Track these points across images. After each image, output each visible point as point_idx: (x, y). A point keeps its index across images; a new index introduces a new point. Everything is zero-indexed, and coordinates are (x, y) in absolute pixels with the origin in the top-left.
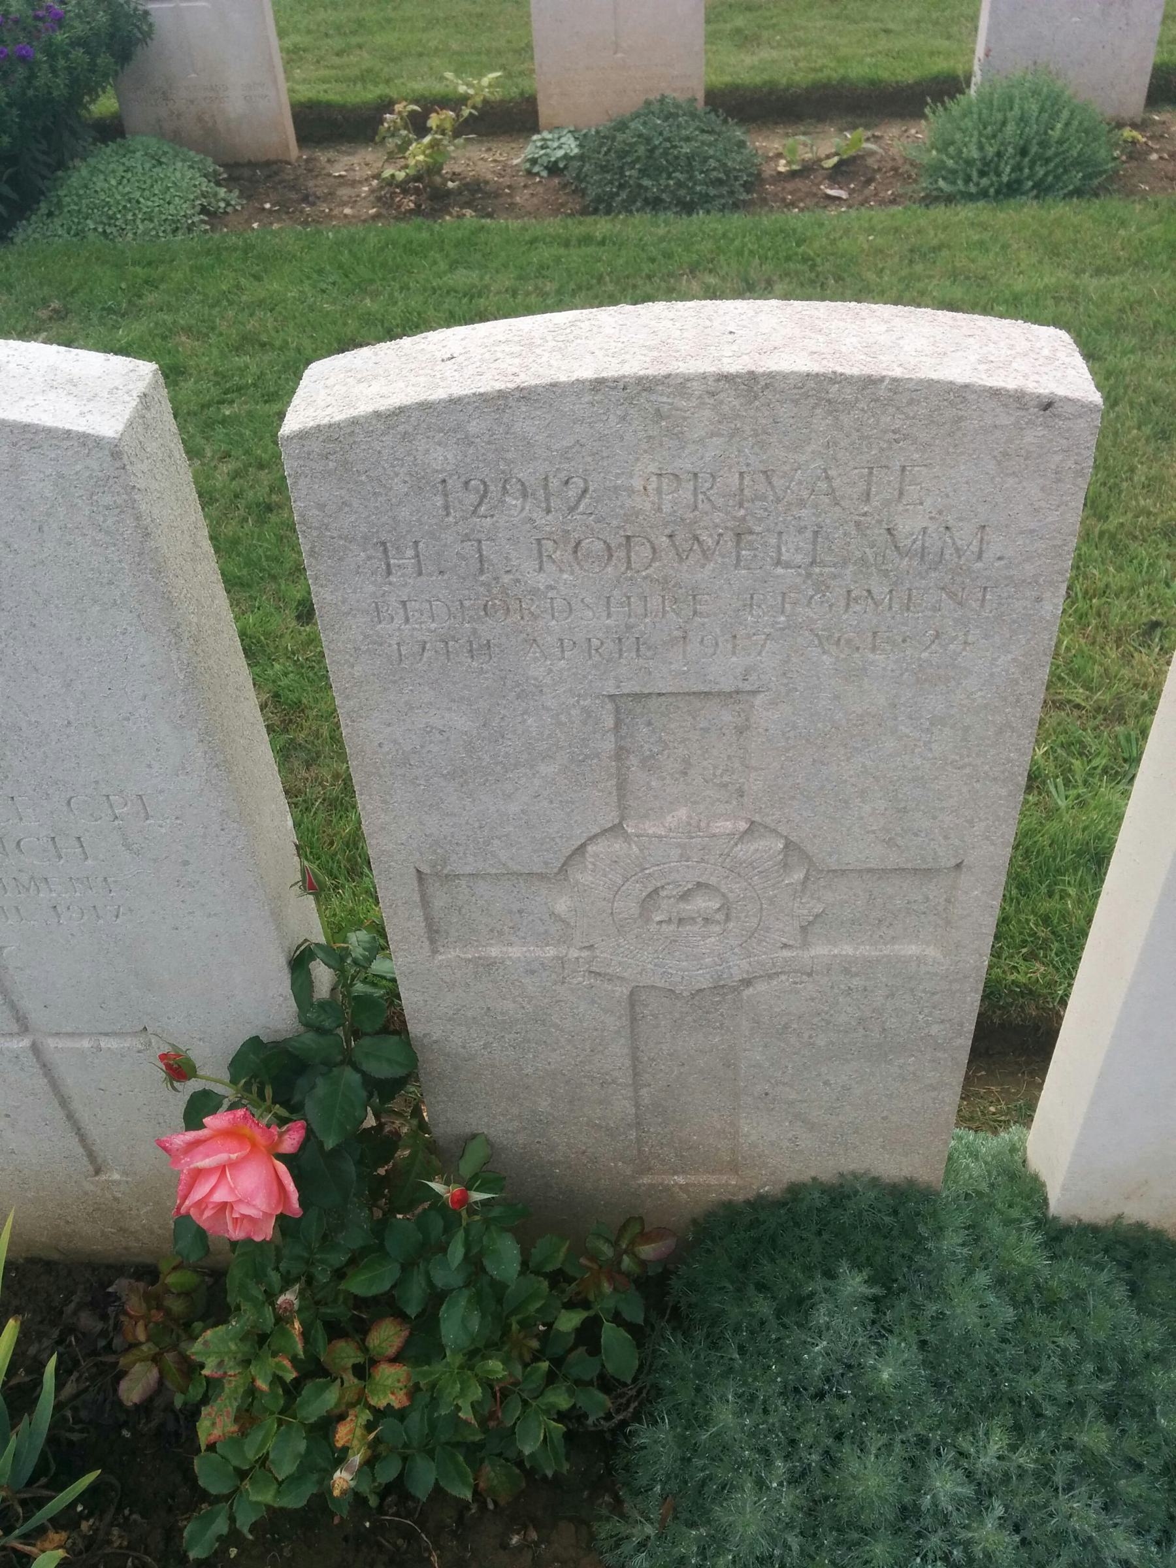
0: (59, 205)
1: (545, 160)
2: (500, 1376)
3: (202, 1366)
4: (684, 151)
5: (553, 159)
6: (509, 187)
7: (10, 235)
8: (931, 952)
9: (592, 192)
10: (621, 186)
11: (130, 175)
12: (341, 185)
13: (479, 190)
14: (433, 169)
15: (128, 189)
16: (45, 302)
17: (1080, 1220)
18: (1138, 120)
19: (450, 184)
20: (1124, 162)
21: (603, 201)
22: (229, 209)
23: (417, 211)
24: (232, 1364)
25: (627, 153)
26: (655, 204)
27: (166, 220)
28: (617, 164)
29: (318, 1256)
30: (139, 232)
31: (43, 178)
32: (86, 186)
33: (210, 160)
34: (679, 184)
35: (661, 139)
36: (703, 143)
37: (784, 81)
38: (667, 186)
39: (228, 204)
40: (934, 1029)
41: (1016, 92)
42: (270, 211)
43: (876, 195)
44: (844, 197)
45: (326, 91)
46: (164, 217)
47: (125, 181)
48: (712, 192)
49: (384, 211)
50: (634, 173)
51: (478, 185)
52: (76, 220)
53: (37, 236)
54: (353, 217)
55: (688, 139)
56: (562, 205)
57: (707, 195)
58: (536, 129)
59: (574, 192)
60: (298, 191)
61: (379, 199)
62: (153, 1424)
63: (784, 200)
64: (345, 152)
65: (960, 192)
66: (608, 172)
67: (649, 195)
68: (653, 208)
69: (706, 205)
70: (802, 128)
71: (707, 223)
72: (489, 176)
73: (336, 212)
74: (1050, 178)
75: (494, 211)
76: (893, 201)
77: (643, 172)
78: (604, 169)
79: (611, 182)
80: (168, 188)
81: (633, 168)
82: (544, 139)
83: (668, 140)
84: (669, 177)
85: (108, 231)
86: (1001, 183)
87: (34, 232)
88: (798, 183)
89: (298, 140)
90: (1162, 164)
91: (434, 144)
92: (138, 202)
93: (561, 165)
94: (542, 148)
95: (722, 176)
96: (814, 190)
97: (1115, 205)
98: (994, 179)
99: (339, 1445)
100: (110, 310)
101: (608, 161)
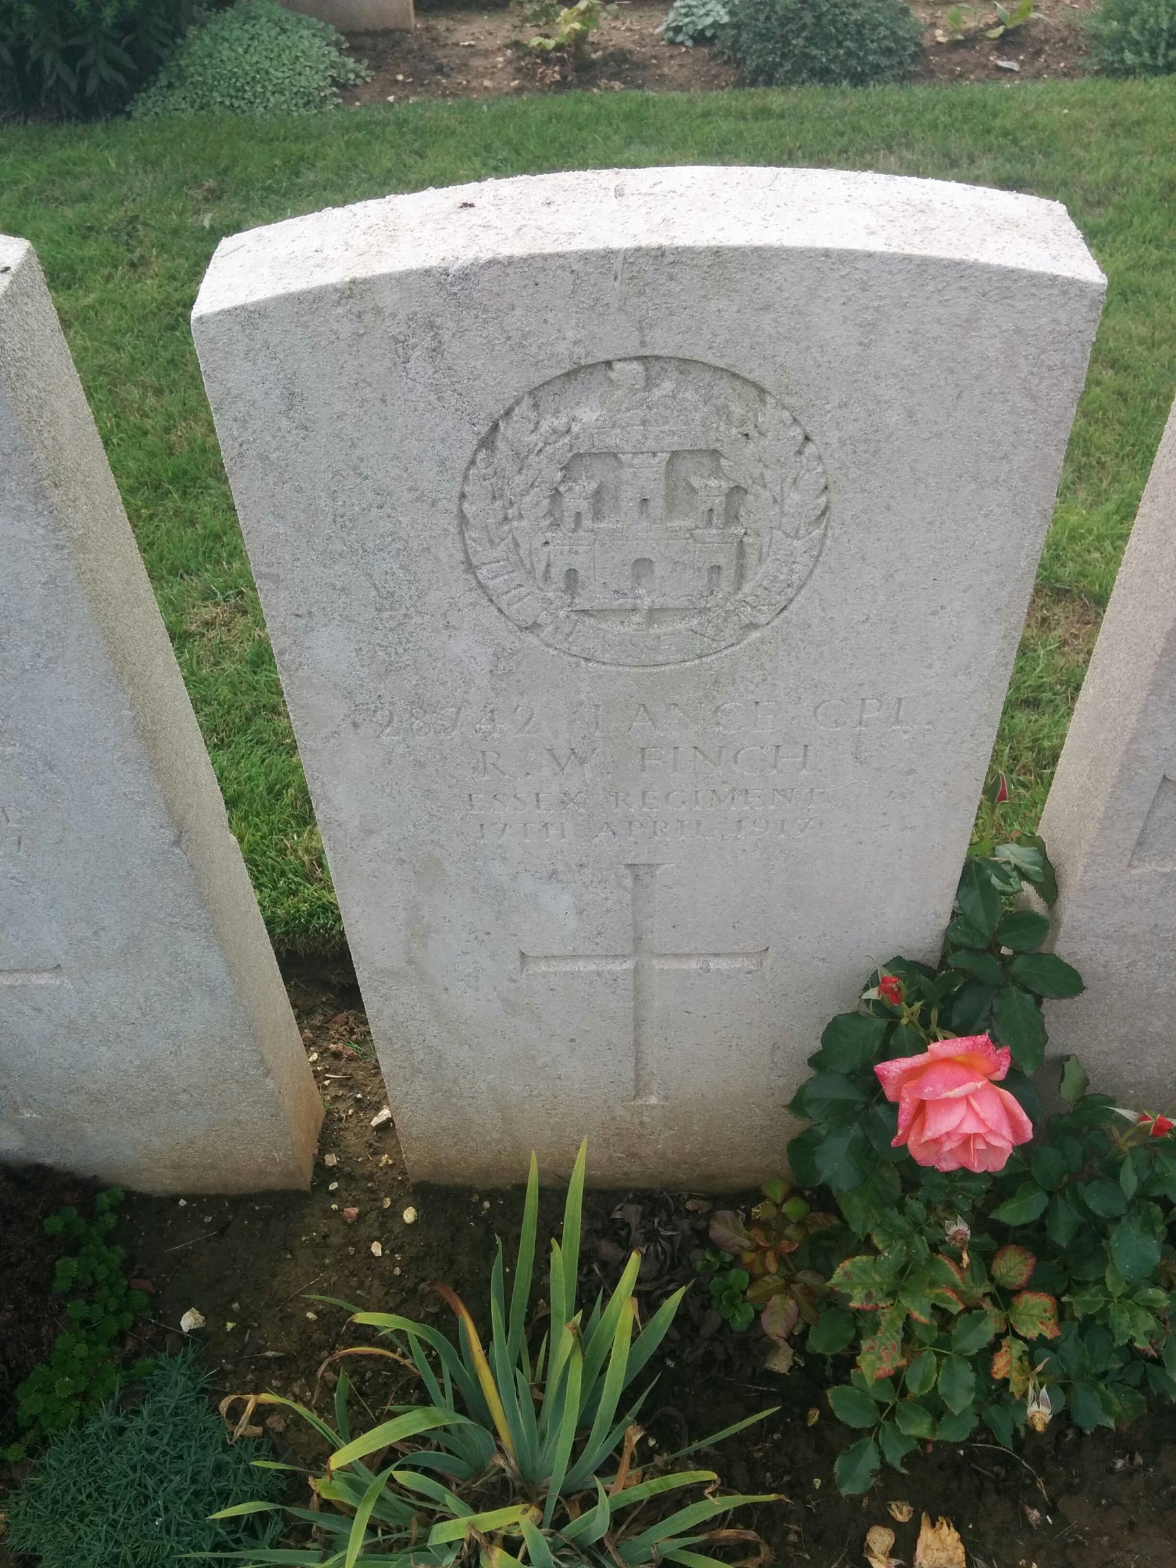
0: (181, 77)
1: (690, 29)
2: (1165, 1305)
3: (850, 1298)
4: (853, 18)
5: (700, 27)
6: (655, 57)
7: (127, 109)
9: (751, 63)
11: (256, 43)
13: (626, 60)
14: (579, 38)
15: (255, 59)
16: (197, 181)
21: (763, 72)
22: (359, 81)
23: (562, 85)
24: (880, 1295)
26: (823, 75)
27: (296, 94)
28: (778, 32)
29: (960, 1185)
30: (270, 105)
31: (164, 46)
32: (210, 56)
33: (332, 27)
34: (850, 54)
38: (837, 56)
39: (357, 76)
42: (404, 83)
43: (1048, 67)
46: (295, 90)
47: (252, 50)
48: (884, 62)
49: (527, 84)
50: (801, 42)
52: (200, 92)
53: (158, 110)
54: (495, 89)
56: (716, 77)
57: (878, 66)
59: (726, 62)
60: (430, 61)
61: (519, 70)
62: (700, 1352)
63: (952, 72)
64: (461, 20)
66: (769, 41)
67: (818, 65)
68: (820, 80)
69: (876, 77)
71: (885, 94)
72: (631, 46)
78: (763, 37)
80: (297, 58)
81: (798, 37)
84: (840, 45)
85: (236, 104)
87: (154, 106)
92: (267, 73)
93: (708, 34)
94: (686, 15)
95: (892, 45)
96: (983, 60)
99: (998, 1377)
100: (269, 189)
101: (768, 29)
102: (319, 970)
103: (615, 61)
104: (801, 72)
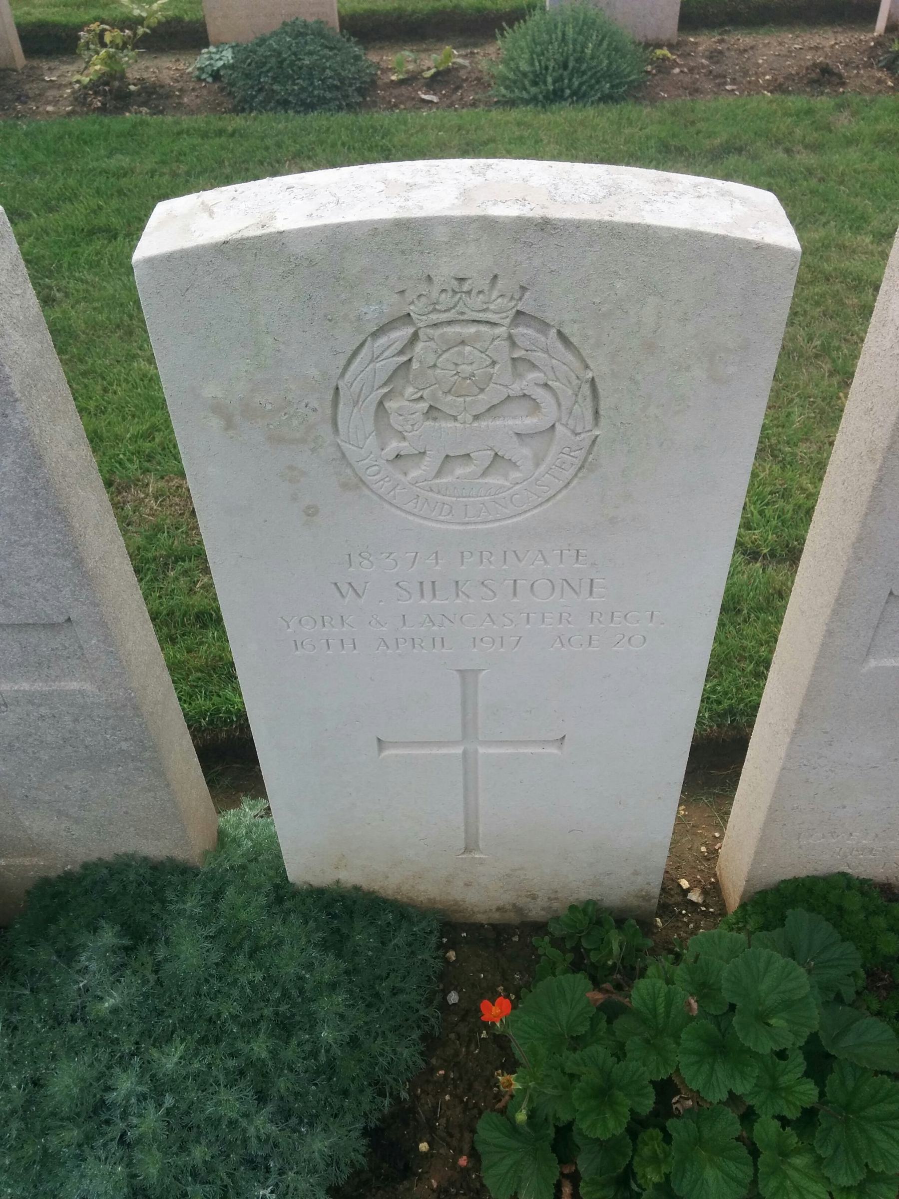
1: (209, 69)
8: (88, 687)
9: (239, 95)
10: (260, 90)
12: (50, 88)
17: (311, 885)
18: (675, 42)
19: (132, 87)
20: (655, 75)
23: (103, 110)
25: (265, 64)
26: (285, 104)
34: (303, 89)
35: (289, 53)
36: (324, 57)
37: (410, 9)
40: (124, 745)
41: (559, 18)
43: (461, 99)
44: (435, 101)
45: (53, 14)
48: (328, 95)
49: (78, 109)
51: (155, 88)
54: (54, 113)
55: (310, 53)
56: (219, 105)
57: (325, 98)
58: (207, 45)
65: (519, 98)
70: (424, 46)
73: (41, 109)
74: (584, 88)
75: (164, 109)
76: (474, 104)
77: (275, 79)
79: (252, 87)
82: (210, 53)
83: (295, 54)
86: (548, 91)
88: (403, 90)
89: (25, 52)
90: (681, 77)
91: (111, 57)
97: (629, 109)
98: (543, 87)
102: (229, 757)
103: (147, 92)
104: (270, 102)
